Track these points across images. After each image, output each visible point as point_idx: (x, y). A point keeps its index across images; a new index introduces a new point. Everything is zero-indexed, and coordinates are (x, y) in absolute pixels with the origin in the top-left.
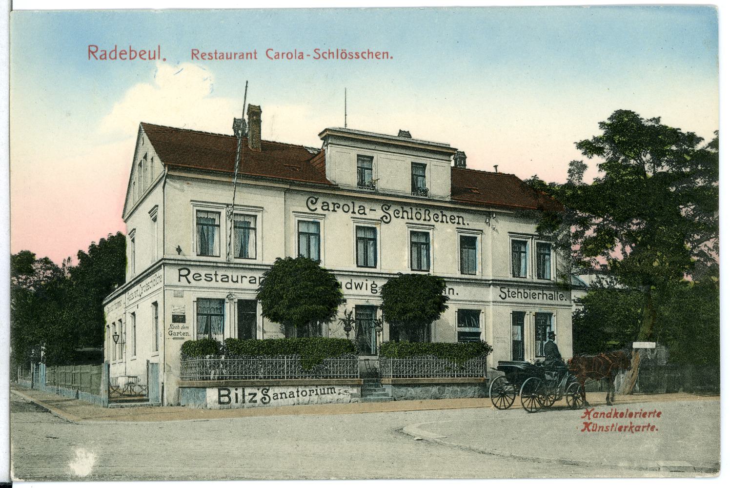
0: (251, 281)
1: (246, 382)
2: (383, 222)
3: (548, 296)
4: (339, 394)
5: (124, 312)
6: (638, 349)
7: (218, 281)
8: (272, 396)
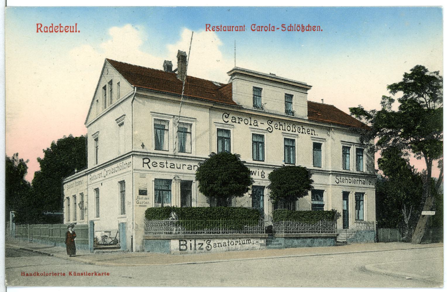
0: (189, 168)
1: (197, 235)
2: (268, 132)
3: (362, 182)
4: (253, 244)
5: (86, 187)
6: (424, 215)
7: (168, 168)
8: (212, 245)
